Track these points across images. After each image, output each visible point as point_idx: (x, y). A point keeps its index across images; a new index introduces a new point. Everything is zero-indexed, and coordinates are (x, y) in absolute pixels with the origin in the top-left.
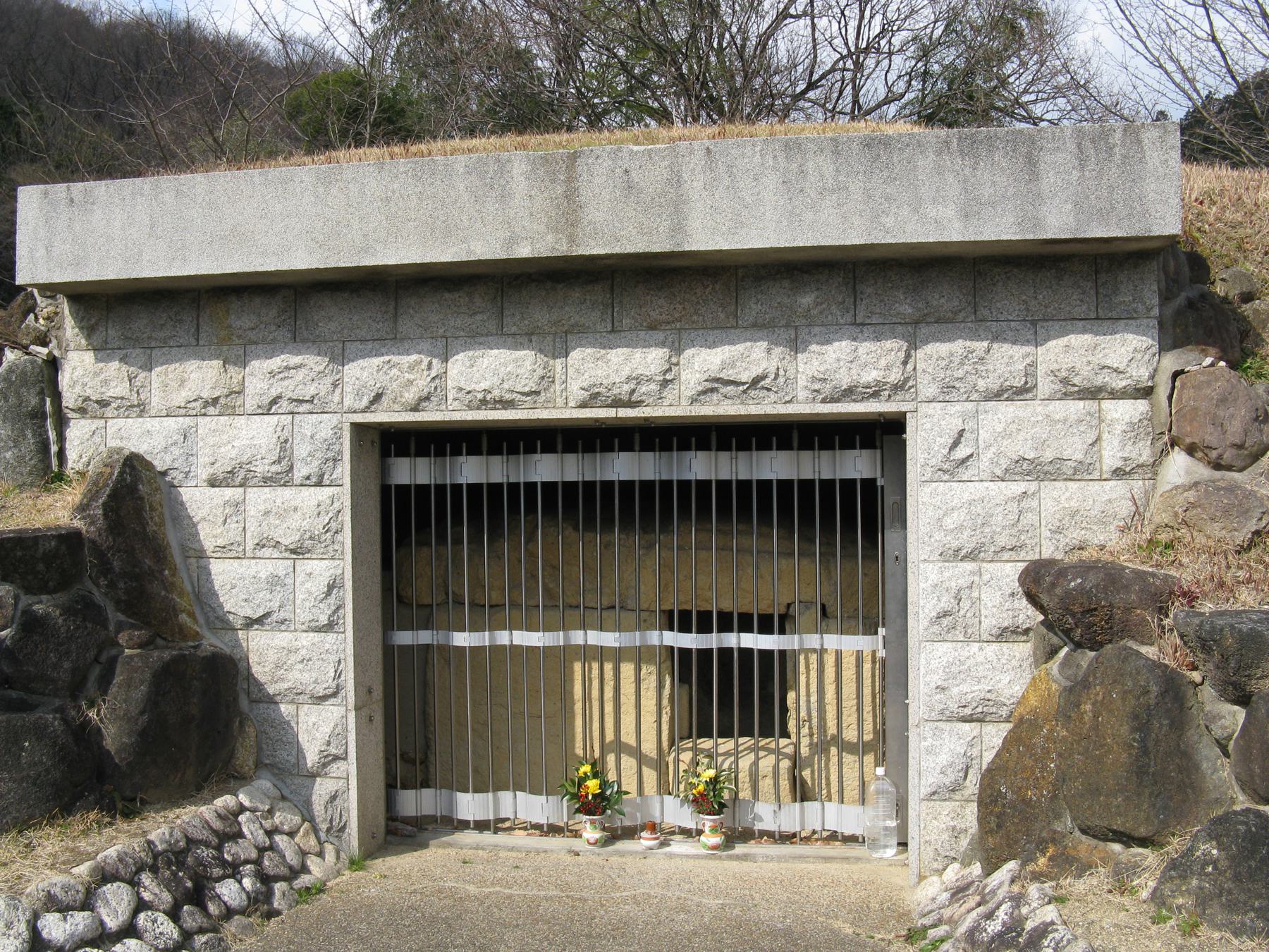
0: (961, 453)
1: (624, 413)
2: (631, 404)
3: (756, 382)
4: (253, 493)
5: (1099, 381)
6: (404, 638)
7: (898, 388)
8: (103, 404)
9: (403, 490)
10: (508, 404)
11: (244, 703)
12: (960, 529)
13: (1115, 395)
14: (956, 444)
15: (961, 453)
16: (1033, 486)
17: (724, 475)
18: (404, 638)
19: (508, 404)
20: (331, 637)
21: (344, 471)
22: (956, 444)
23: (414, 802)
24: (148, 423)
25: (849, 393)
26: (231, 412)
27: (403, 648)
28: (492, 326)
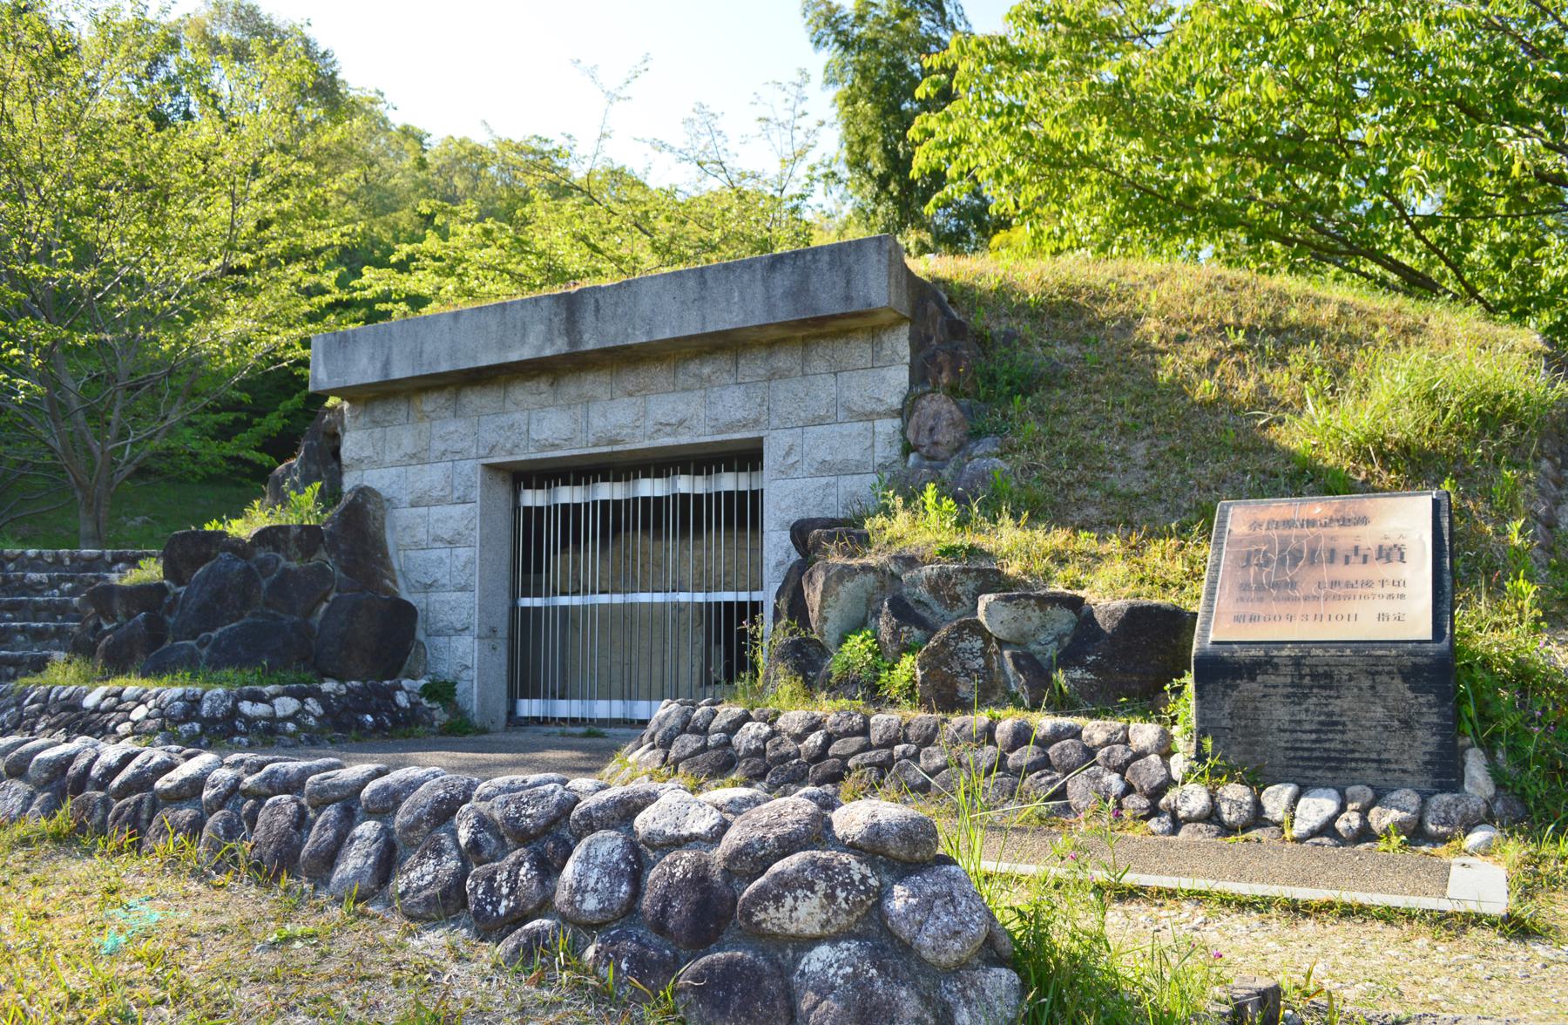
0: (791, 460)
1: (617, 448)
2: (616, 442)
3: (681, 423)
4: (433, 509)
5: (869, 408)
6: (526, 602)
7: (756, 422)
8: (361, 461)
9: (528, 509)
10: (554, 446)
11: (420, 635)
12: (789, 507)
13: (880, 415)
14: (788, 454)
15: (791, 460)
16: (833, 479)
17: (698, 491)
18: (526, 602)
19: (554, 446)
20: (467, 594)
21: (476, 494)
22: (788, 454)
23: (529, 707)
24: (384, 471)
25: (731, 427)
26: (422, 462)
27: (526, 609)
28: (551, 401)
